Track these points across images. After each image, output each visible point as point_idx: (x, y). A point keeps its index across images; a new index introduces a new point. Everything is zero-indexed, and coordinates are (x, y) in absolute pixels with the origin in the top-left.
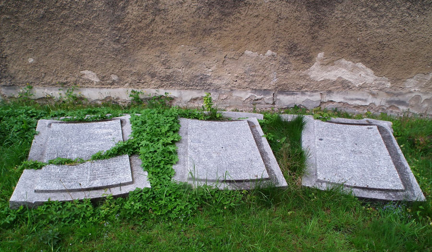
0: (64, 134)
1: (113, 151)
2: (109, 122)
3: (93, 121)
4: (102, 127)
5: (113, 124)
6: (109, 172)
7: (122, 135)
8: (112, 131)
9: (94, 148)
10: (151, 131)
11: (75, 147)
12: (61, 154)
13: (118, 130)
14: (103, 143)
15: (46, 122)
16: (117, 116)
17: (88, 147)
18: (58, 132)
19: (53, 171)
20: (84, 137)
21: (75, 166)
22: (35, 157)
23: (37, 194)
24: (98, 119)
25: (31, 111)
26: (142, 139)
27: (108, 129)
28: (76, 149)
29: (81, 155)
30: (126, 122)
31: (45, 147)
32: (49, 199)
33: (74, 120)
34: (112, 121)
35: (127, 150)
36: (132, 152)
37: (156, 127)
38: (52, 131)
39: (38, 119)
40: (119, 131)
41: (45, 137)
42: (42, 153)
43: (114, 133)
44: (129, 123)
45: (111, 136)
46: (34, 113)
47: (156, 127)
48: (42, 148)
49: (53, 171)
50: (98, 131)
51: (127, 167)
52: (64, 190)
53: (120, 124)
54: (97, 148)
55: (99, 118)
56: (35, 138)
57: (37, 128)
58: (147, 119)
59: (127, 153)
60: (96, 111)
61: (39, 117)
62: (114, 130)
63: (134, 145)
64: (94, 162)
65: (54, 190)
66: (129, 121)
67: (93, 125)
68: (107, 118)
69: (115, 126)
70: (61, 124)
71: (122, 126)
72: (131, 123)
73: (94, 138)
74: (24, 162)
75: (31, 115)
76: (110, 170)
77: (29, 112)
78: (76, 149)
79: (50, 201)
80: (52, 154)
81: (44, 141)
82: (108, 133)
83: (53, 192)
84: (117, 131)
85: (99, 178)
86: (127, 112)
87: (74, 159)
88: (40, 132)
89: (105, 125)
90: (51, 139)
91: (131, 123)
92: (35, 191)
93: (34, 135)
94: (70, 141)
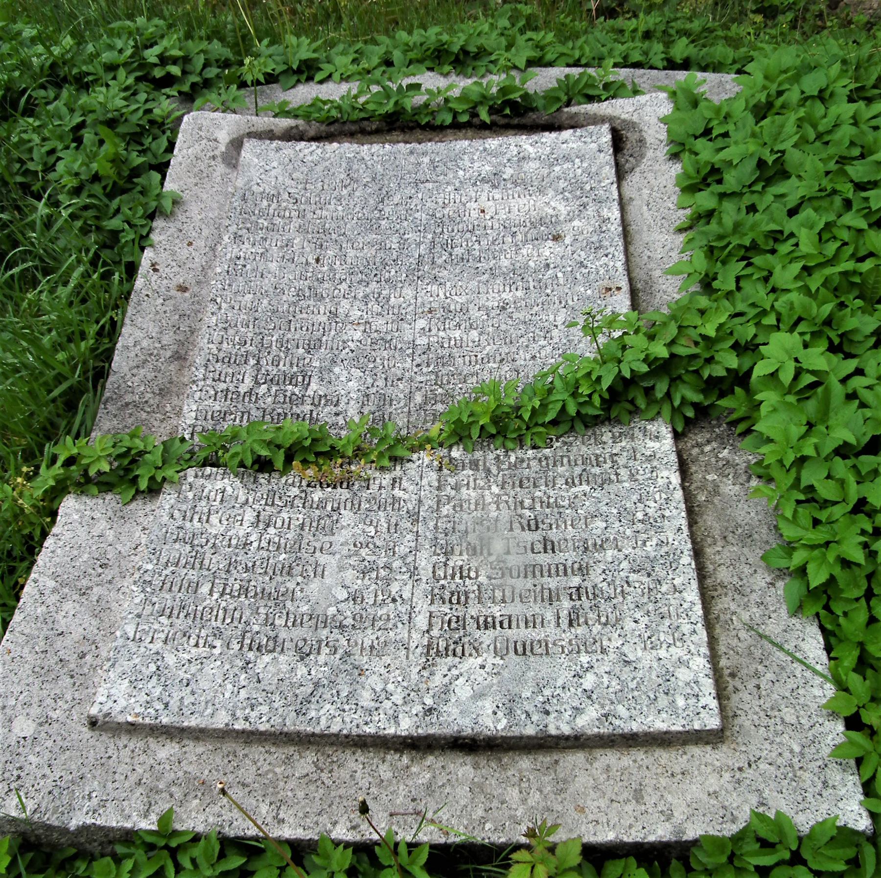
0: (302, 215)
1: (574, 394)
2: (549, 137)
3: (456, 126)
4: (508, 172)
5: (567, 158)
6: (552, 583)
7: (621, 243)
8: (563, 209)
9: (457, 334)
10: (832, 248)
11: (356, 314)
12: (276, 363)
13: (599, 201)
14: (507, 296)
15: (219, 127)
16: (590, 99)
17: (421, 323)
18: (271, 198)
19: (216, 527)
20: (403, 243)
21: (343, 493)
22: (142, 372)
23: (103, 744)
24: (484, 116)
25: (157, 50)
26: (764, 313)
27: (541, 191)
28: (358, 335)
29: (381, 383)
30: (641, 141)
31: (198, 302)
32: (165, 819)
33: (356, 115)
34: (567, 134)
35: (668, 395)
36: (695, 406)
37: (863, 224)
38: (244, 199)
39: (189, 98)
40: (605, 213)
41: (206, 232)
42: (181, 343)
43: (576, 223)
44: (663, 152)
45: (559, 249)
46: (175, 61)
47: (863, 224)
48: (185, 306)
49: (216, 527)
50: (484, 202)
51: (671, 561)
52: (262, 733)
53: (607, 157)
54: (474, 334)
55: (492, 111)
56: (155, 237)
57: (170, 171)
58: (787, 145)
59: (666, 410)
60: (473, 49)
61: (193, 85)
62: (575, 205)
63: (710, 360)
64: (454, 466)
65: (202, 731)
66: (663, 136)
67: (456, 159)
68: (534, 110)
69: (577, 169)
70: (290, 149)
71: (621, 174)
72: (675, 156)
73: (458, 251)
74: (66, 448)
75: (158, 73)
76: (560, 557)
77: (151, 55)
78: (358, 335)
79: (175, 833)
80: (228, 360)
81: (199, 261)
82: (541, 221)
83: (197, 739)
84: (591, 211)
85: (487, 637)
86: (636, 57)
87: (343, 437)
88: (186, 196)
89: (523, 158)
90: (233, 251)
91: (675, 156)
92: (93, 723)
93: (152, 217)
94: (331, 269)
